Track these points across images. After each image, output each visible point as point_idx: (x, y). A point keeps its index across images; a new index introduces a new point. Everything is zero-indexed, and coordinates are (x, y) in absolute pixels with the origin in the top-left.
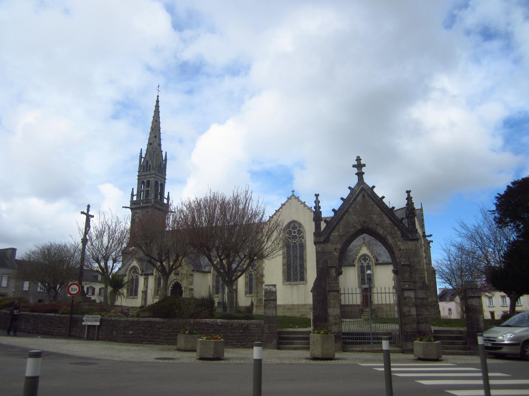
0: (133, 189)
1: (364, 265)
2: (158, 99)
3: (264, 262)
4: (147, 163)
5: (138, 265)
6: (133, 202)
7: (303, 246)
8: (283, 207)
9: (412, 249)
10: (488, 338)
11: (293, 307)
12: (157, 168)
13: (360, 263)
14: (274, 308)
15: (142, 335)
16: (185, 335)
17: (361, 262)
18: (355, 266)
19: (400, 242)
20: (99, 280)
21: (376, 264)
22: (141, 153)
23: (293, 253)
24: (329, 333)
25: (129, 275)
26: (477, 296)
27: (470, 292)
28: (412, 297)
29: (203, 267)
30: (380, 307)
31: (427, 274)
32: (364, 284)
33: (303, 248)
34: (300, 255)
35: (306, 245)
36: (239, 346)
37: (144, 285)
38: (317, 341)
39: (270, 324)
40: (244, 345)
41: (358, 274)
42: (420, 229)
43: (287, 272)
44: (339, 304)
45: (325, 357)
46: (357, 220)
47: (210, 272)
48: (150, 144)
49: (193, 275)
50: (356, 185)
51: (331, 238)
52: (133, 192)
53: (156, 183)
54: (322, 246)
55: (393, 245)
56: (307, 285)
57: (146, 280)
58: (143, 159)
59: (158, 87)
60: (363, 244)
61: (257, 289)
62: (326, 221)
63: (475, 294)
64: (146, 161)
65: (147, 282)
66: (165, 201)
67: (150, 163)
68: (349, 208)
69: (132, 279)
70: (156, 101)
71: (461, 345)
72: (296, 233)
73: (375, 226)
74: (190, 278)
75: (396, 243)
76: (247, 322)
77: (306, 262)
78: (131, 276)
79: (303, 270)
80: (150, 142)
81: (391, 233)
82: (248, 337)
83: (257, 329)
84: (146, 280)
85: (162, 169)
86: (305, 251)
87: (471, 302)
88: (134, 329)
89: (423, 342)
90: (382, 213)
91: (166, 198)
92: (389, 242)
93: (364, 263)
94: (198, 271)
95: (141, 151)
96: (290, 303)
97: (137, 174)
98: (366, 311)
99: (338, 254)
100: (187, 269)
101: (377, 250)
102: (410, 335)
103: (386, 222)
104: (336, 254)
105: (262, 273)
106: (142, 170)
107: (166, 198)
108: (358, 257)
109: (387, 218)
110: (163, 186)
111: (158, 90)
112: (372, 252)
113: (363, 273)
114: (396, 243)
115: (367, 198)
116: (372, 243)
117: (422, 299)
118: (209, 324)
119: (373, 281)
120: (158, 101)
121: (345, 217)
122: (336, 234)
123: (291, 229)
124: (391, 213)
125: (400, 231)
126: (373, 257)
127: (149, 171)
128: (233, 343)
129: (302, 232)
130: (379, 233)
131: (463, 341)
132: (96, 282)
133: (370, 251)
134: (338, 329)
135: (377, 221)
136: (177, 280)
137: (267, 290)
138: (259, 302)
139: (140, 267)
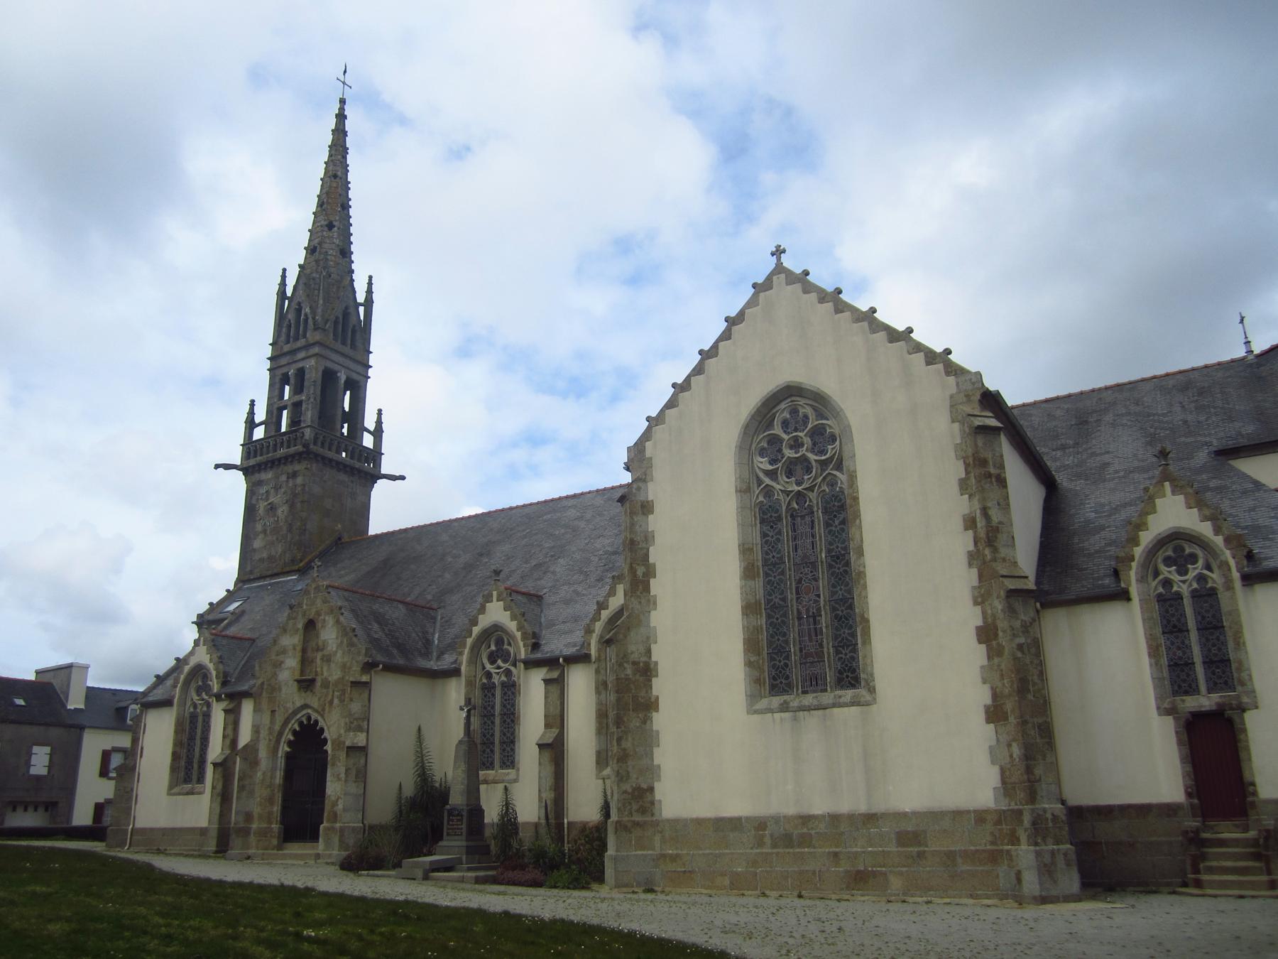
0: (252, 403)
2: (342, 109)
3: (655, 603)
4: (299, 311)
6: (249, 448)
7: (842, 507)
8: (735, 328)
11: (805, 830)
13: (1154, 584)
17: (1161, 577)
18: (1129, 599)
21: (1250, 580)
22: (283, 284)
25: (183, 702)
32: (1186, 693)
33: (842, 516)
34: (829, 551)
35: (856, 499)
37: (224, 737)
41: (1150, 639)
43: (770, 644)
47: (455, 672)
48: (311, 250)
49: (367, 685)
52: (251, 413)
53: (329, 376)
56: (874, 707)
60: (1160, 483)
61: (619, 740)
64: (294, 306)
66: (368, 441)
67: (308, 310)
69: (193, 717)
72: (802, 445)
74: (351, 700)
77: (865, 586)
79: (851, 627)
80: (312, 244)
85: (354, 332)
86: (853, 531)
91: (369, 431)
93: (1176, 577)
94: (390, 669)
96: (791, 810)
97: (268, 351)
98: (1222, 843)
100: (345, 660)
101: (1233, 511)
105: (644, 659)
106: (283, 338)
108: (1138, 551)
110: (357, 388)
111: (344, 83)
112: (1216, 518)
113: (1181, 631)
119: (1239, 669)
123: (777, 430)
126: (1227, 540)
127: (305, 336)
129: (833, 439)
133: (1207, 512)
136: (309, 711)
138: (635, 807)
139: (216, 669)
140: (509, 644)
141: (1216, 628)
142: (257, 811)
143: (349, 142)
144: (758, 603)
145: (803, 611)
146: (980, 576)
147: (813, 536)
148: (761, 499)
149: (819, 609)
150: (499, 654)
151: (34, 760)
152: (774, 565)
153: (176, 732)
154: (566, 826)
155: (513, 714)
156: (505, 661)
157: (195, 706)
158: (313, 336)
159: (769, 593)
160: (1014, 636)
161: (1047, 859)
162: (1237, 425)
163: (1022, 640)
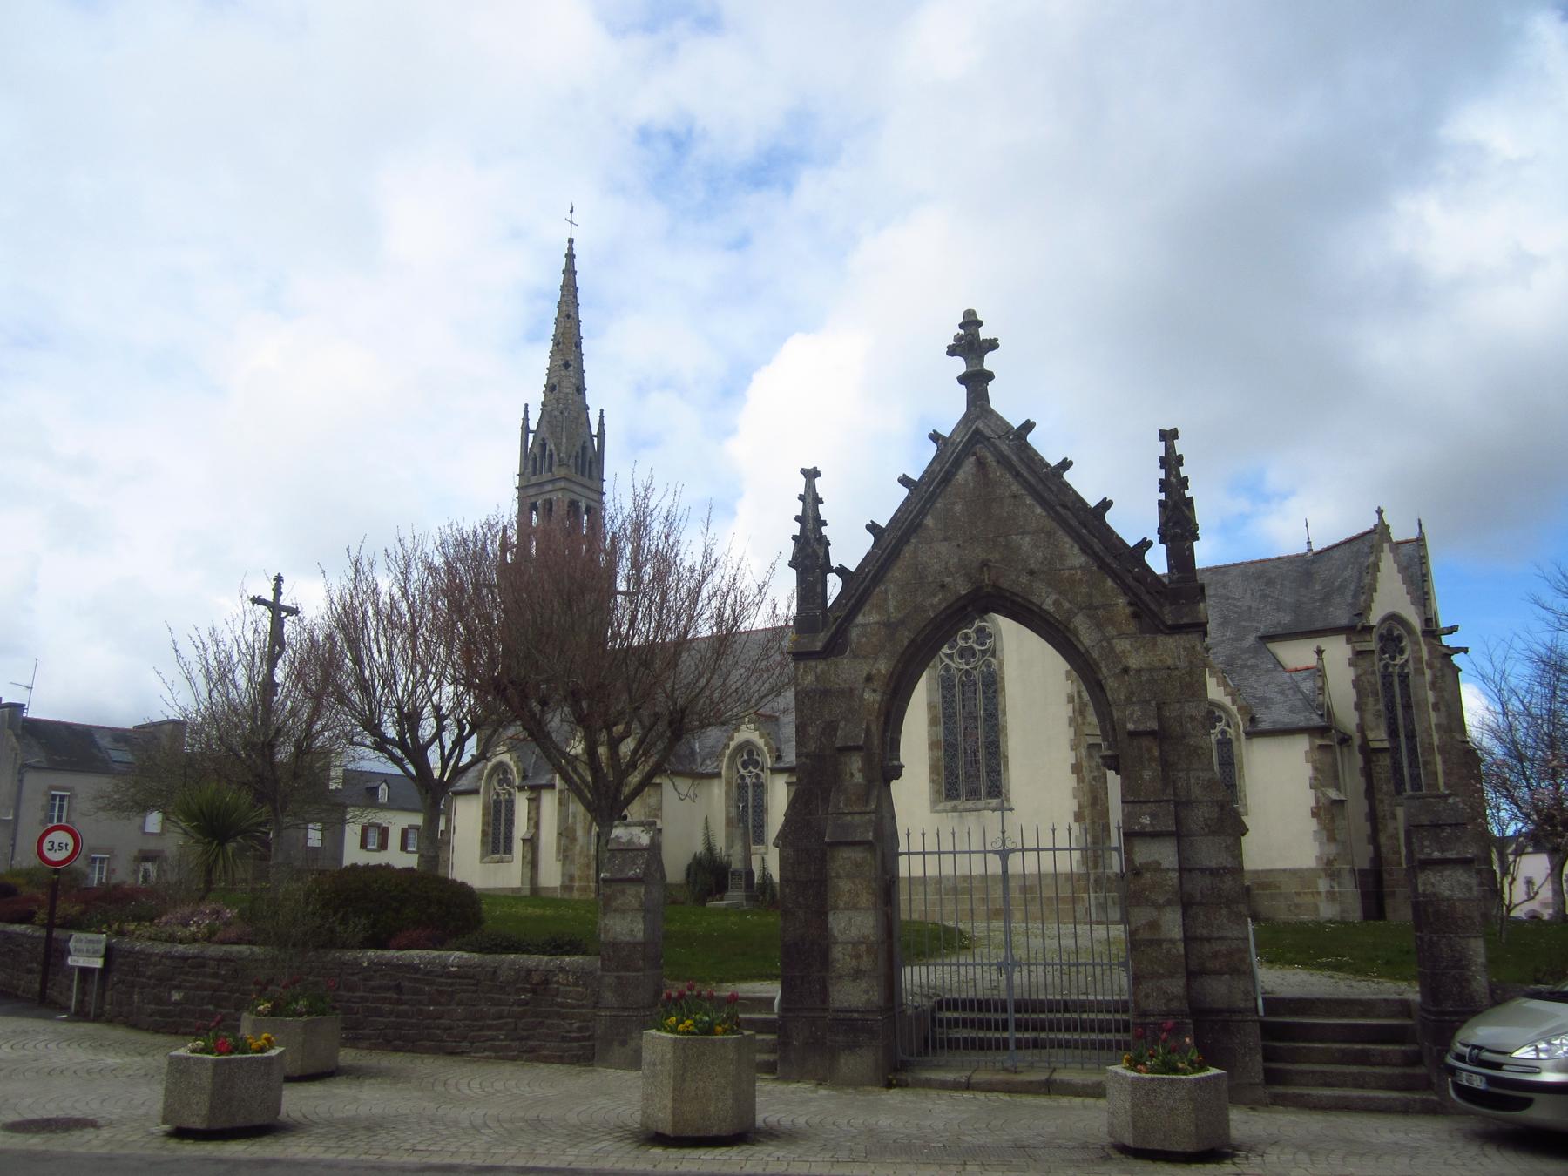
1: (1228, 736)
2: (571, 249)
4: (543, 446)
5: (511, 759)
7: (995, 682)
9: (1177, 669)
10: (1476, 1051)
12: (572, 461)
14: (638, 910)
15: (211, 1007)
16: (253, 1017)
19: (1128, 642)
20: (381, 801)
21: (1250, 735)
22: (526, 419)
23: (964, 708)
24: (719, 1029)
25: (487, 792)
26: (1455, 856)
27: (1427, 843)
28: (1165, 864)
29: (699, 760)
30: (1268, 881)
31: (1444, 762)
34: (985, 710)
35: (1003, 678)
36: (516, 1053)
38: (662, 1063)
39: (622, 974)
40: (532, 1050)
42: (1413, 607)
44: (870, 896)
45: (689, 1132)
46: (956, 560)
47: (718, 775)
48: (551, 388)
50: (958, 426)
51: (854, 634)
53: (573, 505)
54: (818, 670)
55: (1095, 654)
57: (535, 803)
58: (531, 436)
59: (571, 211)
62: (842, 571)
63: (1447, 850)
64: (539, 441)
65: (538, 808)
67: (552, 446)
68: (926, 515)
69: (497, 803)
70: (566, 256)
71: (1395, 1065)
72: (970, 638)
73: (1024, 579)
75: (1109, 643)
76: (547, 963)
77: (1006, 735)
78: (492, 792)
80: (551, 381)
81: (1090, 607)
82: (548, 1021)
83: (580, 989)
84: (535, 803)
85: (590, 462)
87: (1433, 885)
88: (188, 985)
89: (1140, 1072)
90: (1054, 524)
92: (1081, 642)
95: (526, 412)
99: (877, 697)
102: (1155, 1024)
103: (1069, 563)
104: (872, 697)
106: (530, 469)
109: (1072, 547)
111: (571, 223)
114: (1109, 643)
115: (996, 471)
116: (1240, 662)
117: (1213, 872)
118: (420, 969)
120: (570, 257)
121: (907, 551)
122: (874, 618)
124: (1096, 523)
125: (1125, 594)
126: (1239, 709)
127: (550, 469)
128: (497, 1043)
129: (990, 636)
130: (1039, 607)
131: (1403, 1048)
132: (372, 807)
134: (864, 997)
135: (1032, 561)
137: (620, 843)
139: (517, 766)
140: (758, 755)
141: (1230, 764)
142: (577, 873)
143: (579, 282)
144: (939, 741)
145: (968, 748)
146: (1075, 733)
147: (976, 699)
148: (942, 672)
149: (978, 748)
150: (751, 762)
151: (319, 835)
152: (950, 717)
153: (484, 815)
155: (762, 806)
156: (755, 768)
157: (498, 794)
158: (559, 472)
159: (945, 736)
160: (1091, 771)
161: (1101, 900)
162: (1281, 614)
163: (1096, 774)
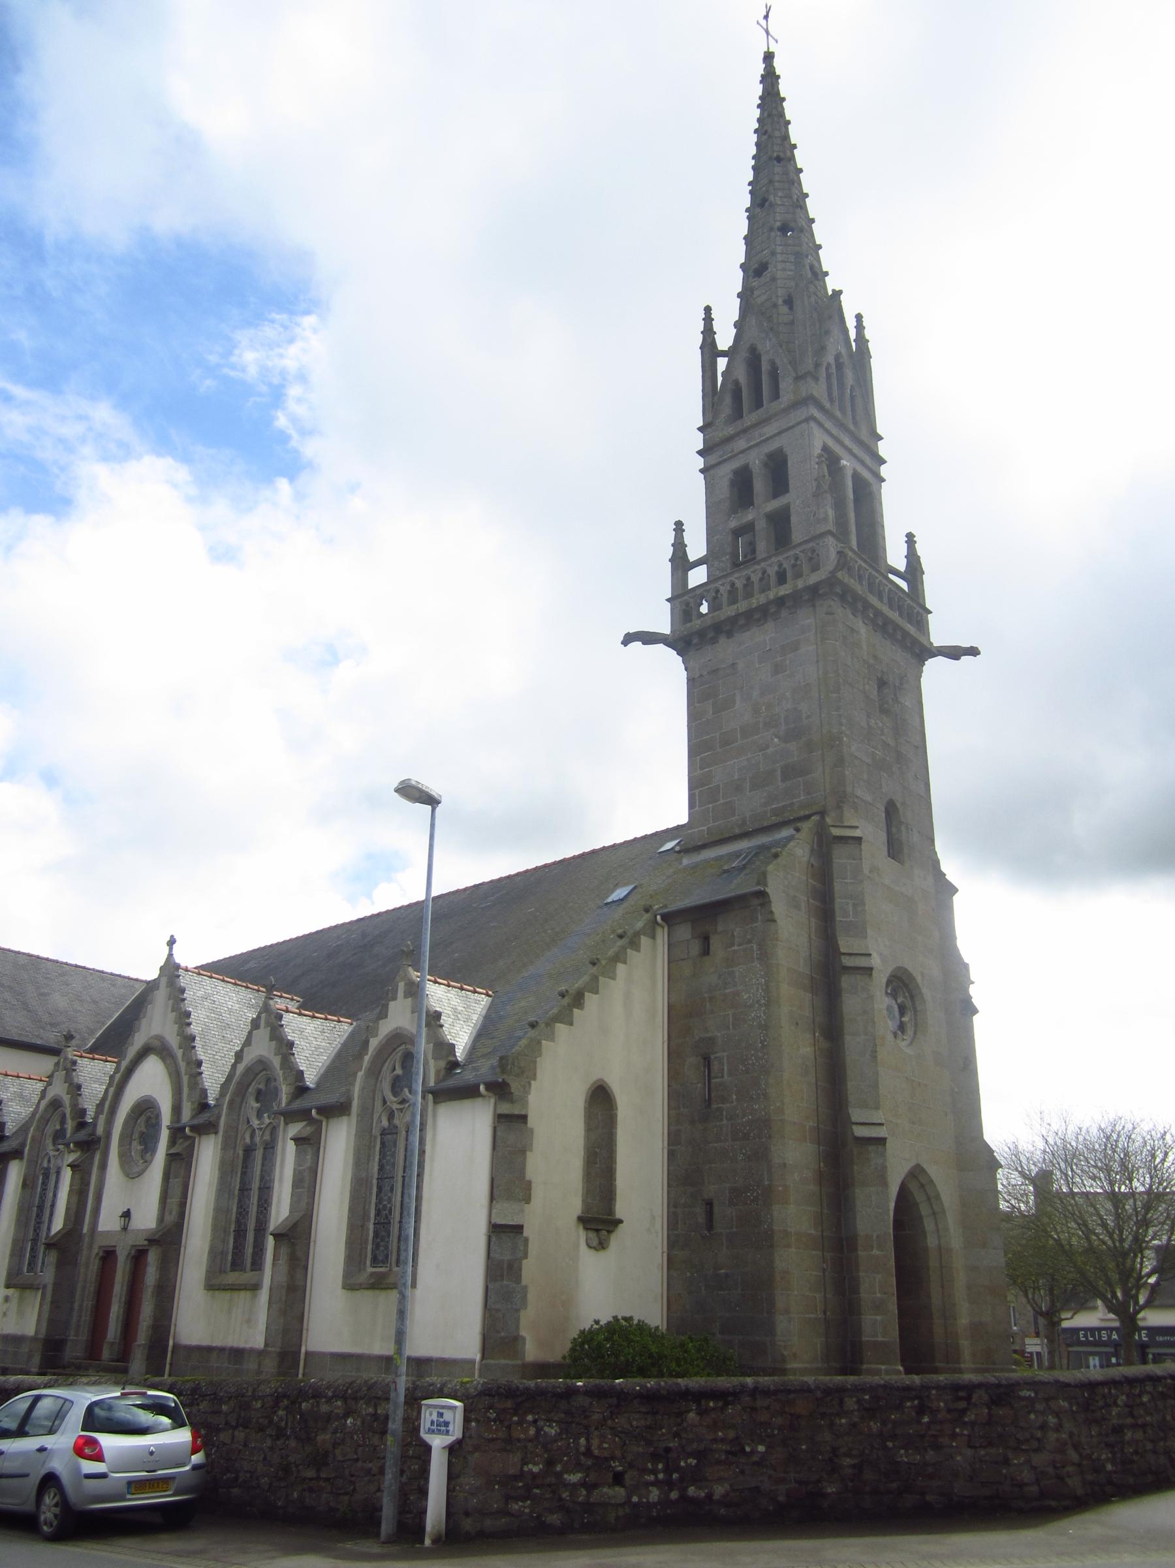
0: (679, 527)
6: (687, 604)
22: (708, 332)
48: (754, 269)
52: (679, 547)
59: (766, 17)
107: (901, 566)
120: (770, 79)
154: (170, 1349)
